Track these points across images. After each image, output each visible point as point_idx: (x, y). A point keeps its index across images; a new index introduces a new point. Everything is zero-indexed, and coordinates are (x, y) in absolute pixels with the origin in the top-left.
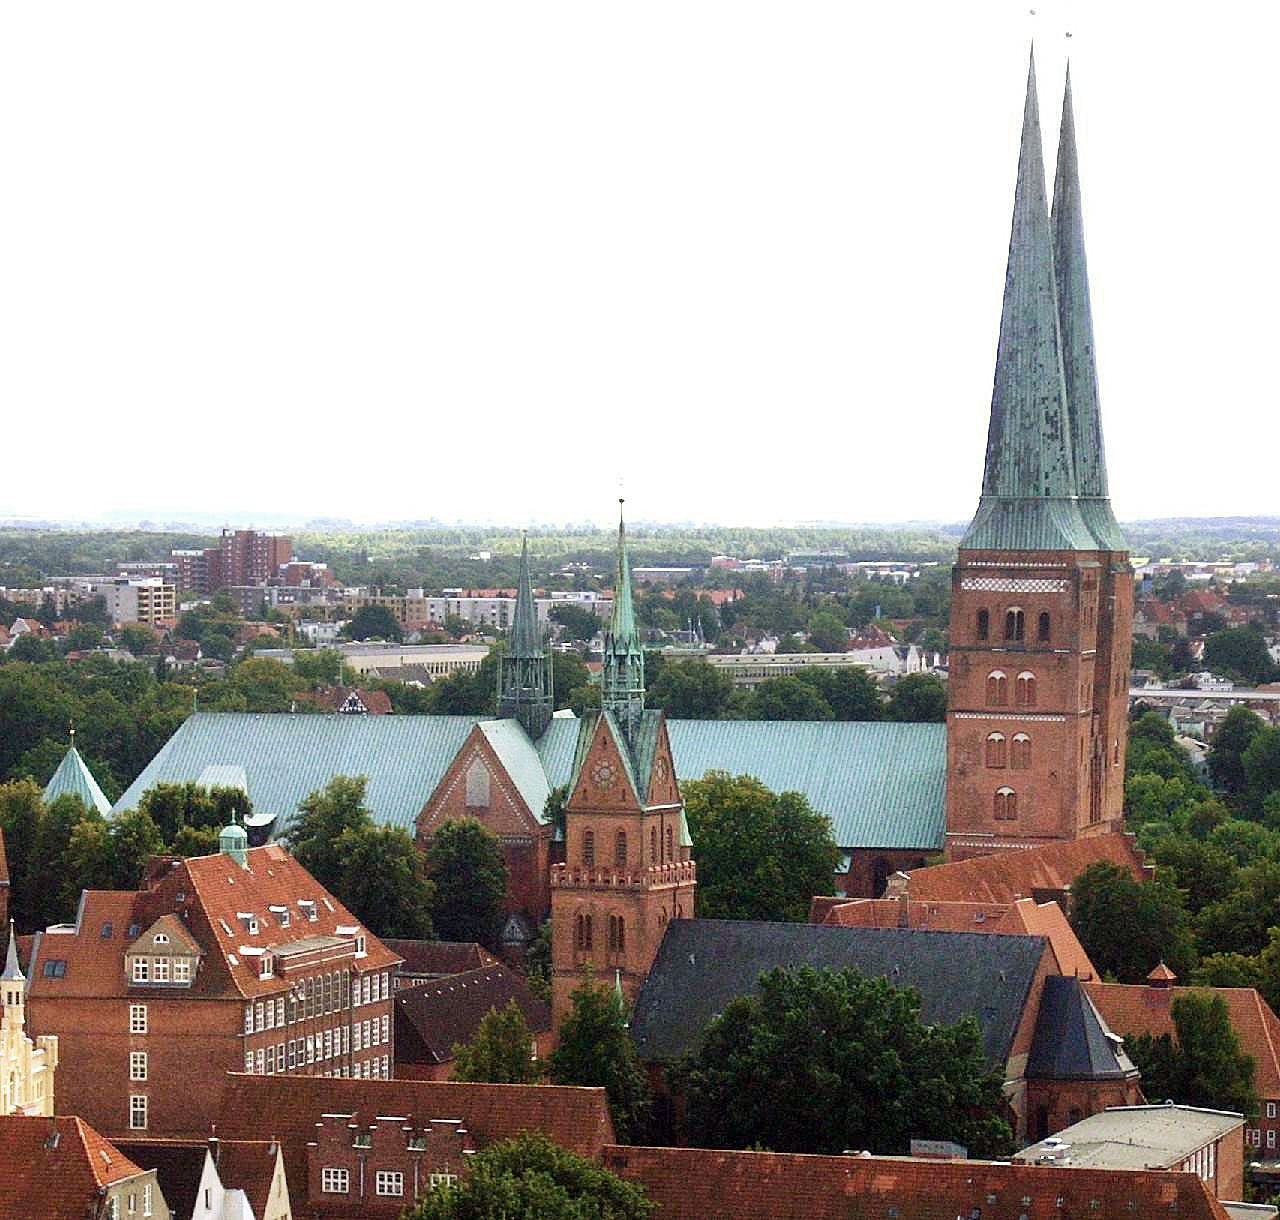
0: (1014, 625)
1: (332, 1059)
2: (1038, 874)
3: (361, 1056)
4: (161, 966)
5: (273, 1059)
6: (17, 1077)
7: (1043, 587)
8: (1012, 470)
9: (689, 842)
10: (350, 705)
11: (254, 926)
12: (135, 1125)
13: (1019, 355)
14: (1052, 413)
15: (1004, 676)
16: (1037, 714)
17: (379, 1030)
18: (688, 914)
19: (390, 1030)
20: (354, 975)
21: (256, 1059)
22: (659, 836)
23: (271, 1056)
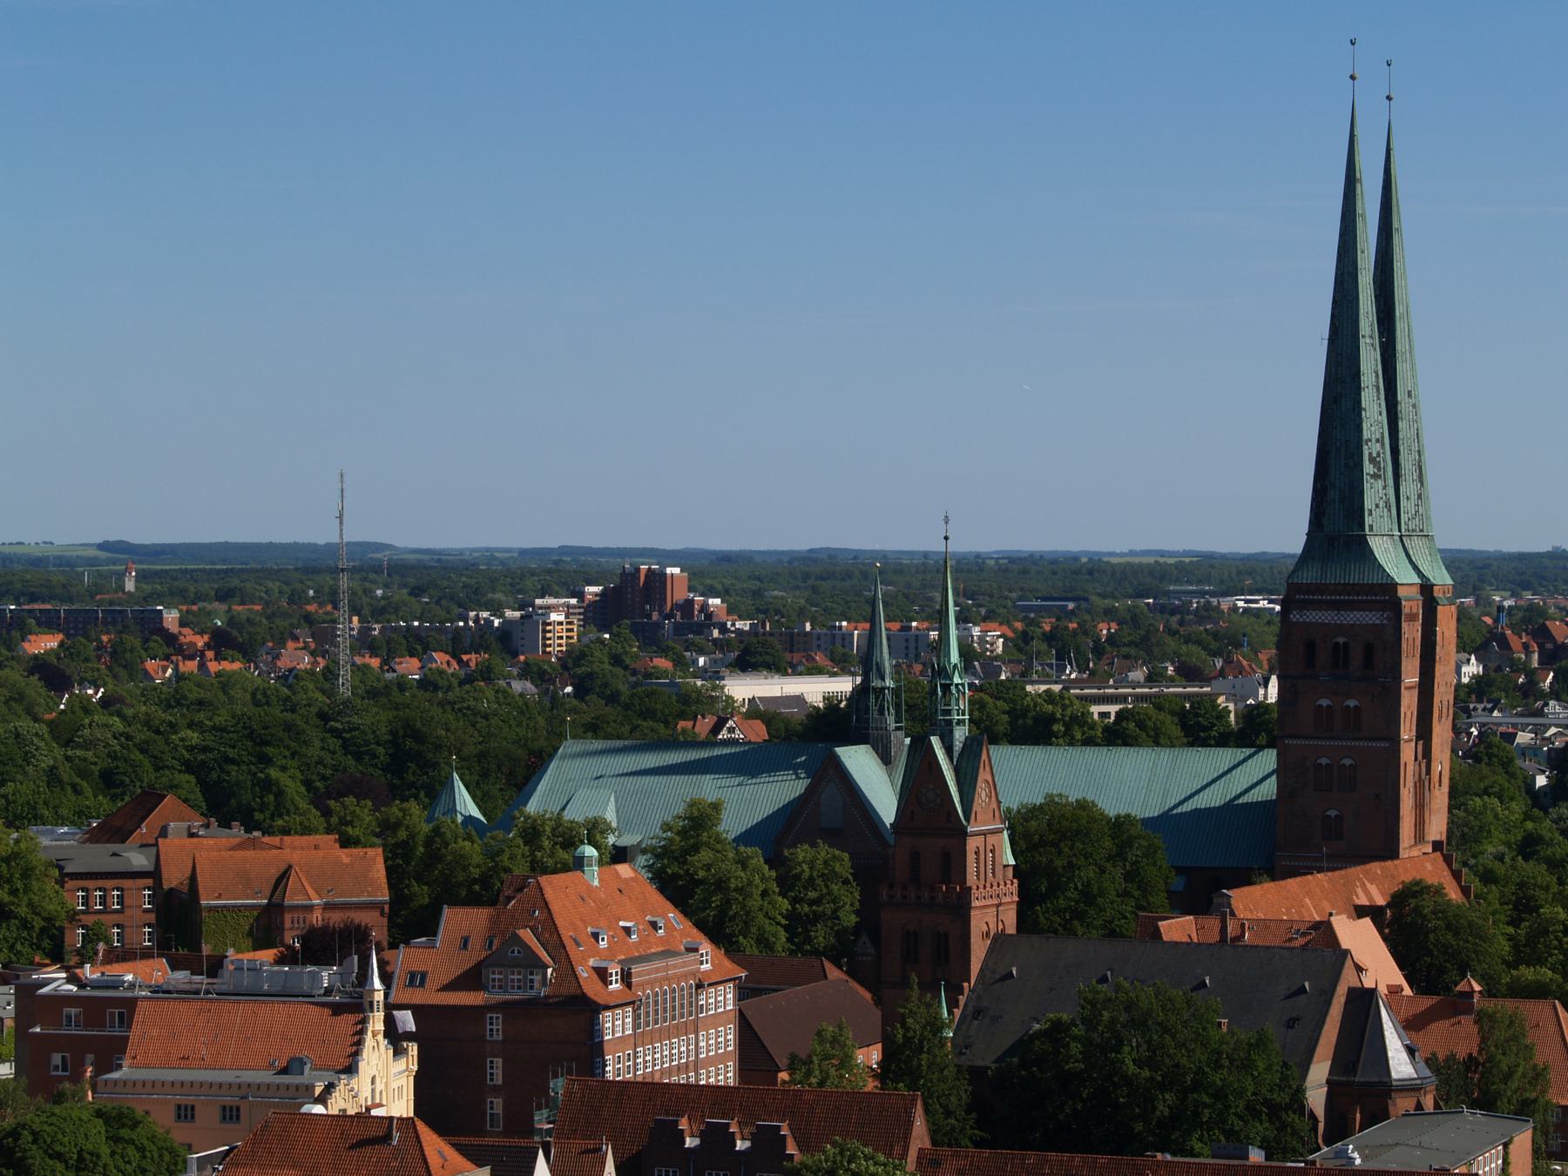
0: (1340, 655)
1: (678, 1067)
2: (1359, 890)
3: (710, 1061)
4: (516, 977)
5: (621, 1066)
6: (378, 1080)
7: (1367, 619)
8: (1337, 507)
9: (1012, 862)
10: (729, 732)
11: (603, 939)
12: (491, 1126)
13: (1343, 398)
14: (1374, 455)
15: (1330, 703)
16: (1361, 739)
17: (724, 1039)
18: (1011, 929)
19: (735, 1040)
20: (699, 986)
21: (662, 1051)
22: (982, 857)
23: (619, 1063)
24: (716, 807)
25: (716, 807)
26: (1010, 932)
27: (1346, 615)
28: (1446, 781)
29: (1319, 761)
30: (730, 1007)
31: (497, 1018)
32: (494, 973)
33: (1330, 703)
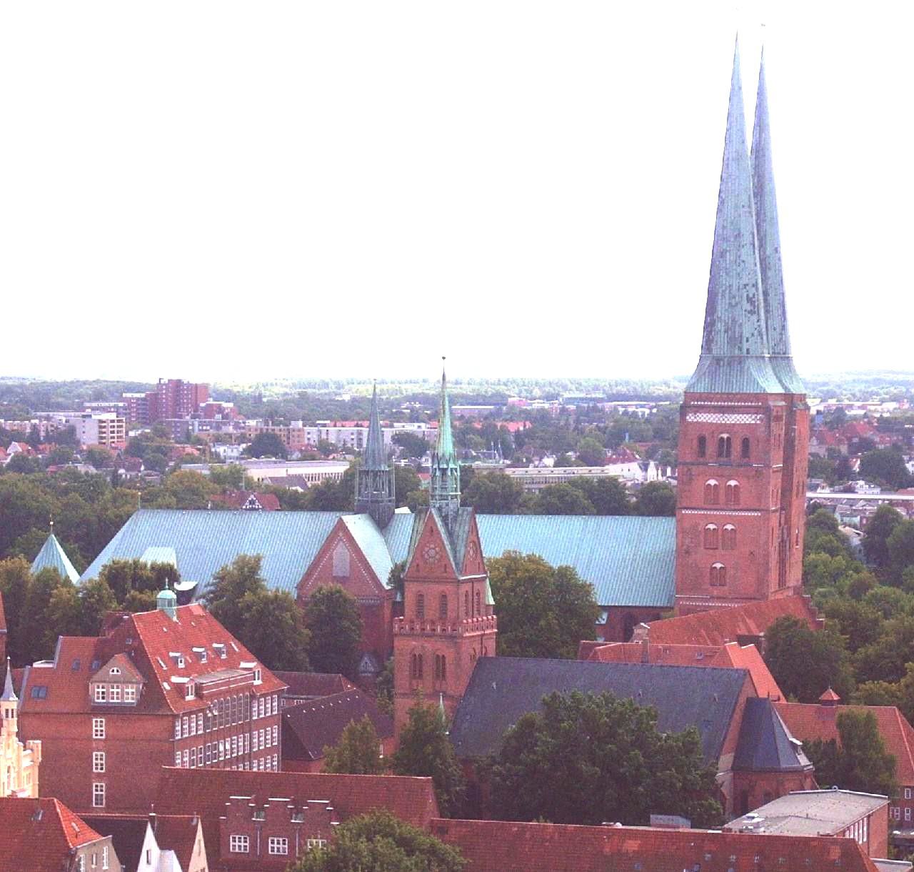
1: (237, 757)
2: (740, 624)
3: (258, 755)
6: (12, 770)
7: (745, 420)
8: (722, 336)
9: (492, 602)
10: (250, 503)
11: (181, 662)
12: (96, 804)
13: (728, 254)
15: (717, 483)
17: (269, 737)
18: (492, 654)
19: (278, 737)
20: (253, 697)
22: (470, 597)
23: (193, 755)
24: (258, 559)
25: (258, 559)
26: (491, 656)
27: (729, 417)
28: (801, 541)
29: (725, 527)
30: (275, 713)
31: (101, 722)
32: (98, 687)
33: (717, 483)
